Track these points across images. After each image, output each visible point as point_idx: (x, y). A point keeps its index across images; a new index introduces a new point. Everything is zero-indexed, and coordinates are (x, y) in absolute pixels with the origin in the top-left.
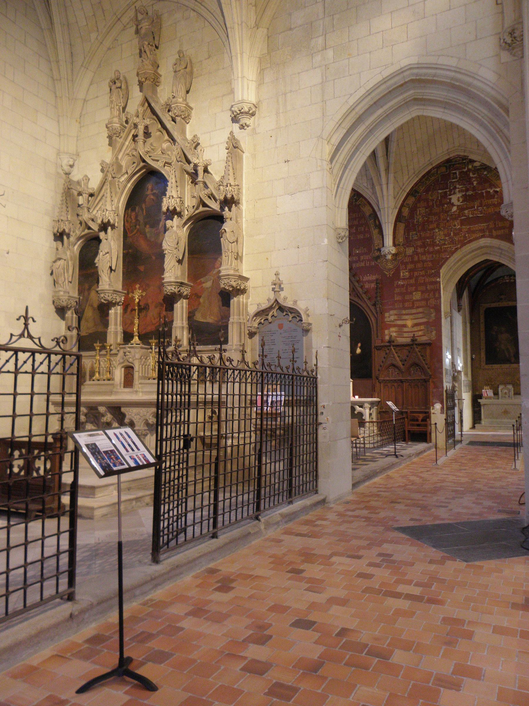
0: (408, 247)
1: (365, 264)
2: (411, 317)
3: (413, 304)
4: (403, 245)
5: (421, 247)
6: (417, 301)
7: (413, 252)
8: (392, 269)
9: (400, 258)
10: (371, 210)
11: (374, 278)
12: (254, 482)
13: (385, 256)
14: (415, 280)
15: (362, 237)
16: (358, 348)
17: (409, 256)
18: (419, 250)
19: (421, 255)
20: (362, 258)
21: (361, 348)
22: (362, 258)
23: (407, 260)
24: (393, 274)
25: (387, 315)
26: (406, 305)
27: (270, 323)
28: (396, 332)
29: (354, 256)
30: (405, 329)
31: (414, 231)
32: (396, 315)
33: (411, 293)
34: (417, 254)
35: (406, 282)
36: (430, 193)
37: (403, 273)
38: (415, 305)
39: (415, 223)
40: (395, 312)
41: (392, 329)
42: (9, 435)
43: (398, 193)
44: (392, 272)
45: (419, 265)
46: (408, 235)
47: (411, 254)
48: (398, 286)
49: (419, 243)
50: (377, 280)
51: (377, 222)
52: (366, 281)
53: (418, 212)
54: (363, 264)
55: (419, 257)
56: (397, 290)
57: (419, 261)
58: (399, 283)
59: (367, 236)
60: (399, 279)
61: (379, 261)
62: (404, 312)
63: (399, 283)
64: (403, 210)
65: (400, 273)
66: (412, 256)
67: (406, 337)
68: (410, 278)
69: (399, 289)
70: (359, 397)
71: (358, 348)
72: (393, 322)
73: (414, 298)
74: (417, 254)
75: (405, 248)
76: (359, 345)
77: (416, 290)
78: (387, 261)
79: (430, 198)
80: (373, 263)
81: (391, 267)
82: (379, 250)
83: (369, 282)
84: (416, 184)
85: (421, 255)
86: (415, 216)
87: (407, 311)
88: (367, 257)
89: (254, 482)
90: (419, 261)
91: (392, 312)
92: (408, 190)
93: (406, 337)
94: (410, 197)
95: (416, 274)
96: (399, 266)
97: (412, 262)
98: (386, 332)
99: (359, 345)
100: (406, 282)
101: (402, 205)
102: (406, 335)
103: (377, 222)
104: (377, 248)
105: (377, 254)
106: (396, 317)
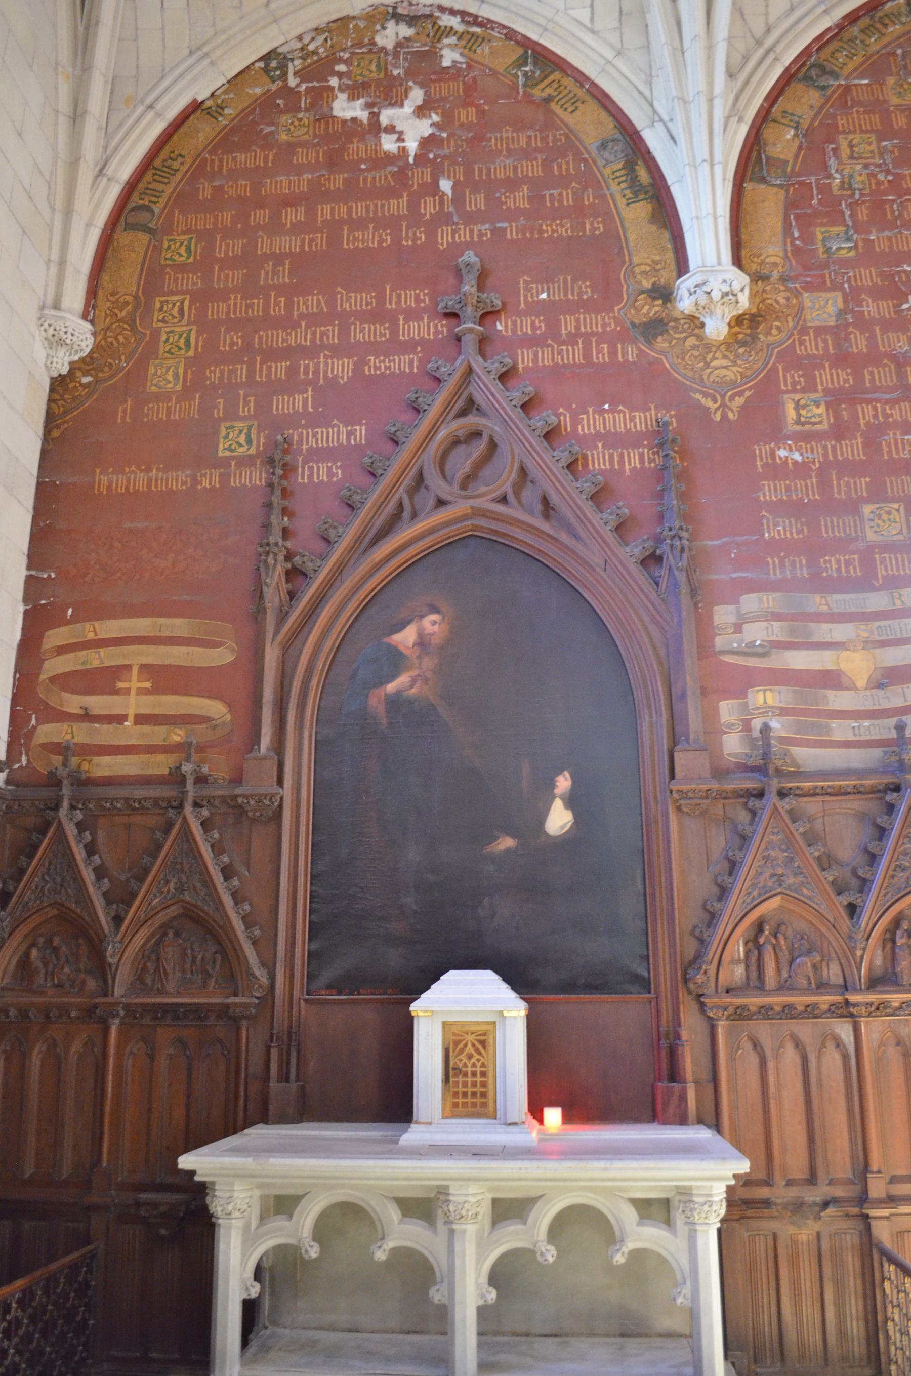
0: (808, 287)
1: (587, 354)
2: (862, 631)
3: (868, 561)
4: (783, 279)
5: (877, 294)
6: (888, 547)
7: (841, 313)
8: (733, 384)
9: (775, 336)
10: (610, 123)
11: (641, 421)
12: (157, 99)
13: (695, 323)
14: (866, 445)
15: (565, 229)
16: (558, 805)
17: (820, 331)
18: (870, 308)
19: (884, 331)
20: (567, 324)
21: (571, 802)
22: (567, 324)
23: (811, 347)
24: (744, 408)
25: (723, 615)
26: (831, 565)
27: (43, 308)
28: (784, 712)
29: (527, 313)
30: (838, 700)
31: (834, 224)
32: (777, 617)
33: (852, 507)
34: (863, 324)
35: (816, 454)
36: (891, 81)
37: (798, 406)
38: (881, 572)
39: (836, 191)
40: (771, 601)
41: (760, 697)
42: (717, 649)
43: (746, 59)
44: (740, 401)
45: (884, 376)
46: (807, 237)
47: (832, 322)
48: (777, 470)
49: (868, 276)
50: (662, 426)
51: (643, 174)
52: (598, 436)
53: (845, 151)
54: (574, 355)
55: (872, 338)
56: (769, 492)
57: (873, 358)
58: (782, 453)
59: (593, 226)
60: (776, 434)
61: (661, 343)
62: (817, 602)
63: (782, 453)
64: (769, 133)
65: (778, 405)
66: (839, 332)
67: (847, 744)
68: (839, 432)
69: (782, 485)
70: (567, 1119)
71: (558, 805)
72: (763, 655)
73: (871, 536)
74: (863, 324)
75: (797, 294)
76: (564, 783)
77: (877, 494)
78: (708, 346)
79: (895, 100)
80: (631, 353)
81: (730, 374)
82: (664, 294)
83: (613, 440)
84: (821, 42)
85: (884, 331)
86: (833, 163)
87: (839, 601)
88: (593, 323)
89: (157, 99)
90: (873, 358)
91: (750, 602)
92: (788, 58)
93: (847, 744)
94: (797, 88)
95: (866, 414)
96: (774, 370)
97: (841, 359)
98: (727, 710)
99: (564, 783)
100: (816, 454)
101: (764, 117)
102: (841, 730)
103: (643, 174)
104: (647, 284)
105: (651, 309)
106: (778, 632)
